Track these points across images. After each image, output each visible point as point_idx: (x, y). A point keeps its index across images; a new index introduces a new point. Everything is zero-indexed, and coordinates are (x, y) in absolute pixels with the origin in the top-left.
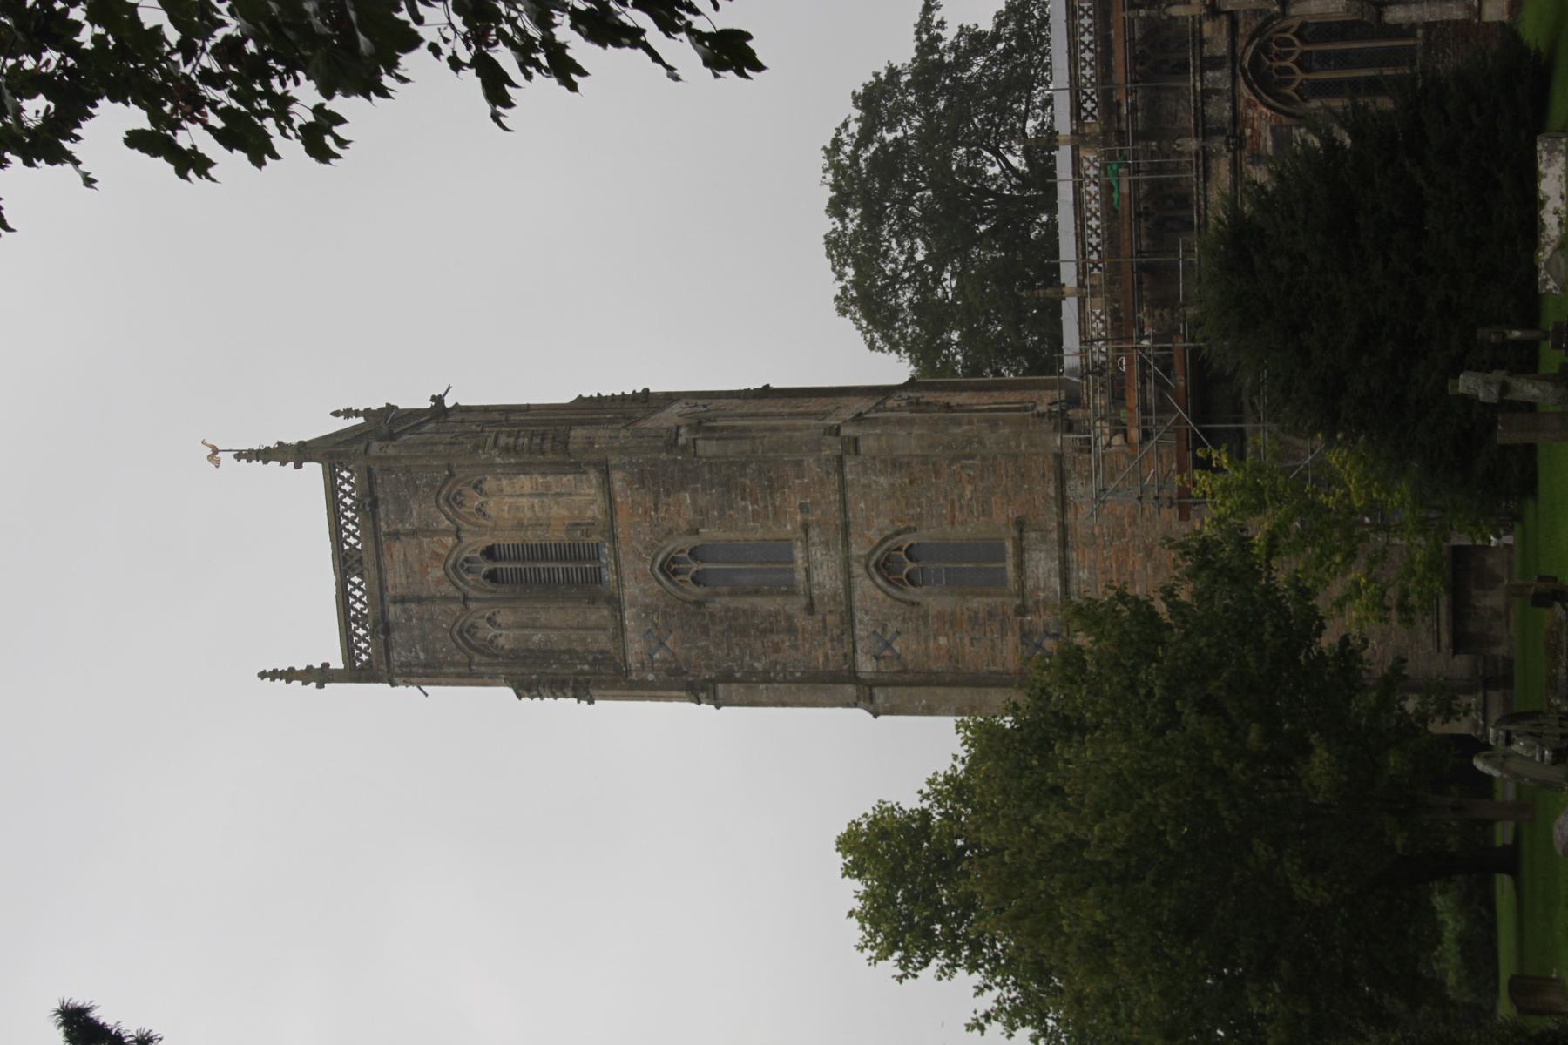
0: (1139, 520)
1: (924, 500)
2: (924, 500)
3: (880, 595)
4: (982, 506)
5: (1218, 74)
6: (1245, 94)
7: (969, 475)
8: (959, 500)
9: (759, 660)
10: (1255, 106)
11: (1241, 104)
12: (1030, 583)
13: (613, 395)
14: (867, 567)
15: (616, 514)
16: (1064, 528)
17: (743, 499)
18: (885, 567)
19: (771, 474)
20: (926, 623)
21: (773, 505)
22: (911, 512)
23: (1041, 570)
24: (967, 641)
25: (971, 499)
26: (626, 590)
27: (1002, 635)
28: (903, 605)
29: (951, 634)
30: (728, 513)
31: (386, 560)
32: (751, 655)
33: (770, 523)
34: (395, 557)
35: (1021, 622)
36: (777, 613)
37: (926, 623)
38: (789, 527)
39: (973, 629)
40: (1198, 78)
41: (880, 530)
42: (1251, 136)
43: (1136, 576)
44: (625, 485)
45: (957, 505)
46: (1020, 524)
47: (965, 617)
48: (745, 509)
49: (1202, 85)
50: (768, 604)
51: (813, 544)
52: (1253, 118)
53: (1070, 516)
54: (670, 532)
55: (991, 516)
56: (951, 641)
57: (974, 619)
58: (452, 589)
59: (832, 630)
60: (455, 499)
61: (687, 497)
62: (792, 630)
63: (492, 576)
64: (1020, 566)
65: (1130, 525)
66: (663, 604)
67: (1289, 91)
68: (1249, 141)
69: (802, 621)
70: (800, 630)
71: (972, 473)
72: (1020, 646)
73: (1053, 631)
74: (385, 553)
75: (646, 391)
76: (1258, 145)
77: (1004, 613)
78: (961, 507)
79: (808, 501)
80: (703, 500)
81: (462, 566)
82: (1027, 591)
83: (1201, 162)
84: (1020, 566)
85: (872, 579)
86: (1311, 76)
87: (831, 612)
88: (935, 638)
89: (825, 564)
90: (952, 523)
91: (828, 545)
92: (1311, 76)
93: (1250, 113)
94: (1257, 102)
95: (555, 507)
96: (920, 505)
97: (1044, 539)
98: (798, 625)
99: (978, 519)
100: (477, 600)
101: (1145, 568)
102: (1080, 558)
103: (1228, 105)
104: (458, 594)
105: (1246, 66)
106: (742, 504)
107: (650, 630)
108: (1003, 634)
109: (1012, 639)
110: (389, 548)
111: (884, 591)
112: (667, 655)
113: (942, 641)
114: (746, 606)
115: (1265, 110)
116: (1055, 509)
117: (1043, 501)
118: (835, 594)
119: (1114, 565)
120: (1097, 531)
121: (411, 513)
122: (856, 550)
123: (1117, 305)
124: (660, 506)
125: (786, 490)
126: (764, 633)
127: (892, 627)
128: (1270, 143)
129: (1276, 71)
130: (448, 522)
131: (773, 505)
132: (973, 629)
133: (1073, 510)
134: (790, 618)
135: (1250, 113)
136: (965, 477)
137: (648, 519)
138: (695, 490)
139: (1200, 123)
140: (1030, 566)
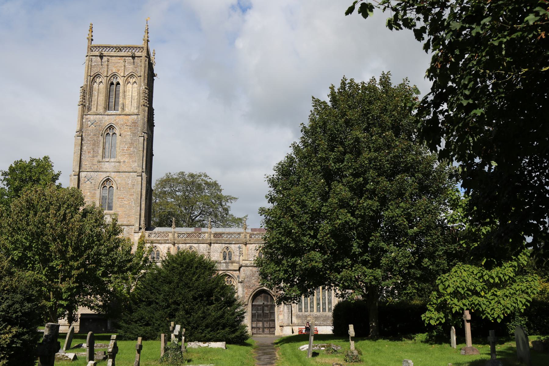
20: (93, 190)
37: (93, 190)
48: (125, 147)
61: (129, 133)
62: (93, 157)
63: (112, 84)
69: (96, 160)
75: (154, 126)
80: (128, 137)
106: (126, 147)
112: (89, 125)
113: (89, 194)
127: (93, 181)
134: (97, 156)
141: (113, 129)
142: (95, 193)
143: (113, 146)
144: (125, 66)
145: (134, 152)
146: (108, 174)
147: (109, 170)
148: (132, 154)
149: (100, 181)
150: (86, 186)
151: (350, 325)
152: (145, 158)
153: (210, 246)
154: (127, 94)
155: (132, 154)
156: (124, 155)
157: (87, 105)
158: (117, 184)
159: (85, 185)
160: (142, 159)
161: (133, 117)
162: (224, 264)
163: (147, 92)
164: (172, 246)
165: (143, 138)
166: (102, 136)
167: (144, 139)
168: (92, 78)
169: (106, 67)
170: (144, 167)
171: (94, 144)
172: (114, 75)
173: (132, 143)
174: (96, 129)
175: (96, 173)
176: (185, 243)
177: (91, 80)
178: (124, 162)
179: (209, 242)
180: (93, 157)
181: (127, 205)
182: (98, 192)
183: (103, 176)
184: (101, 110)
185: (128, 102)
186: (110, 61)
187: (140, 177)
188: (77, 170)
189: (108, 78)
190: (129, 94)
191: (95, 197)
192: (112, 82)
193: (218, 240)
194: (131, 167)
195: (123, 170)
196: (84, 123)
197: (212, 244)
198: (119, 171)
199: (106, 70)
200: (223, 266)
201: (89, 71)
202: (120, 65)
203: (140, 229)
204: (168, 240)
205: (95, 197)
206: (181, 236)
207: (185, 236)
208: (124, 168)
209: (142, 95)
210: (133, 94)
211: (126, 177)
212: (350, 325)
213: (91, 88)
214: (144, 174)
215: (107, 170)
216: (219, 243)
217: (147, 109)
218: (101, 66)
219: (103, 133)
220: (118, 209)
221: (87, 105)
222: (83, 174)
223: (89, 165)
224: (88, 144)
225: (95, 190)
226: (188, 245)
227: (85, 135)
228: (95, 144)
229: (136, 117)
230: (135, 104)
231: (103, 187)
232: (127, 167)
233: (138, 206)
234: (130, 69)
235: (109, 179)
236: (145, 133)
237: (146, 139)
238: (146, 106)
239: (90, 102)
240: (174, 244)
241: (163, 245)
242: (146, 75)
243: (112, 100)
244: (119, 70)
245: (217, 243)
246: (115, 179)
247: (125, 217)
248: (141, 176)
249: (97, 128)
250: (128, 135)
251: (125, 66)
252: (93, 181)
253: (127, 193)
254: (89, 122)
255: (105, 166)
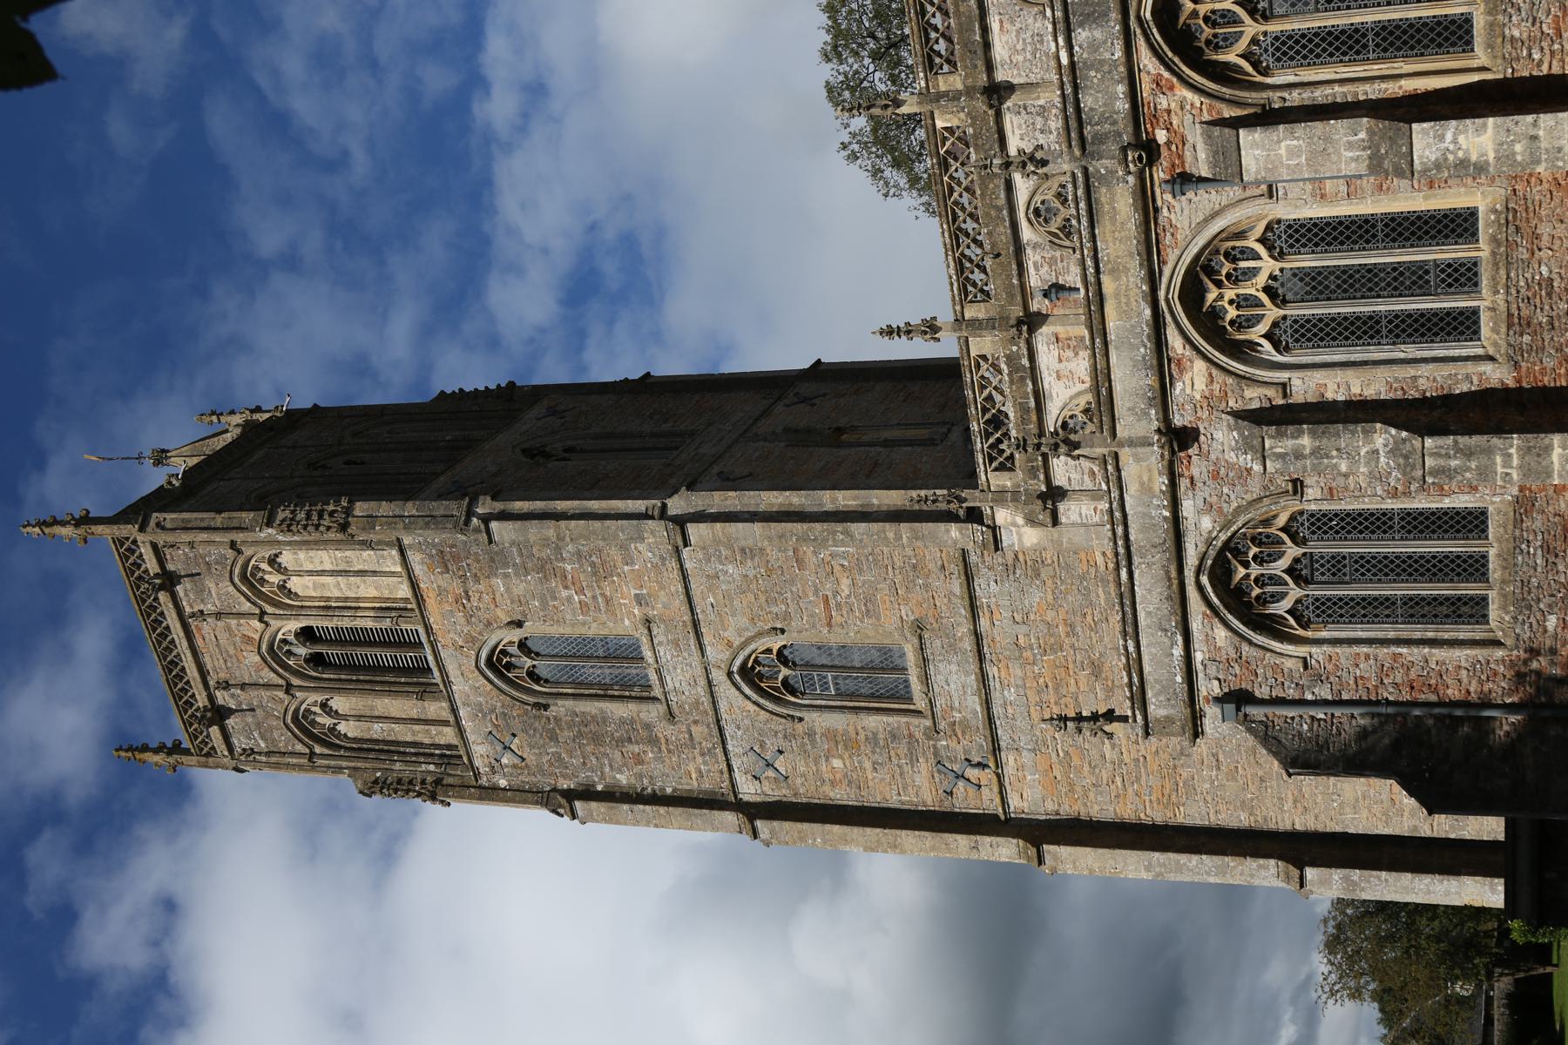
0: (1079, 629)
1: (789, 595)
2: (789, 595)
3: (752, 707)
4: (865, 605)
5: (1098, 34)
6: (1150, 67)
7: (842, 566)
8: (834, 596)
9: (621, 772)
10: (1171, 88)
11: (1146, 87)
12: (940, 703)
13: (476, 389)
14: (730, 674)
15: (424, 601)
16: (978, 637)
17: (566, 587)
18: (750, 674)
19: (594, 558)
20: (813, 742)
21: (603, 595)
22: (775, 609)
23: (953, 686)
24: (868, 765)
25: (849, 596)
26: (454, 688)
27: (911, 760)
28: (783, 720)
29: (846, 756)
30: (550, 603)
31: (199, 642)
32: (611, 766)
33: (604, 617)
34: (207, 640)
35: (935, 747)
36: (632, 721)
37: (813, 742)
38: (627, 622)
39: (873, 752)
40: (1061, 41)
41: (739, 633)
42: (1168, 143)
43: (1081, 698)
44: (425, 568)
45: (832, 602)
46: (919, 628)
47: (862, 737)
48: (569, 599)
49: (1071, 55)
50: (619, 710)
51: (660, 643)
52: (1169, 112)
53: (984, 623)
54: (489, 624)
55: (878, 619)
56: (848, 764)
57: (873, 739)
58: (272, 675)
59: (700, 743)
60: (253, 575)
61: (498, 583)
62: (653, 741)
63: (317, 660)
64: (926, 679)
65: (1068, 635)
66: (499, 704)
67: (1231, 57)
68: (1164, 152)
69: (664, 730)
70: (663, 741)
71: (846, 563)
72: (936, 775)
73: (976, 759)
74: (197, 635)
75: (511, 384)
76: (1181, 157)
77: (911, 736)
78: (838, 605)
79: (645, 591)
80: (519, 588)
81: (280, 648)
82: (938, 709)
83: (1080, 192)
84: (926, 679)
85: (738, 689)
86: (1274, 27)
87: (696, 722)
88: (827, 760)
89: (679, 666)
90: (829, 625)
91: (678, 645)
92: (1274, 27)
93: (1163, 102)
94: (1175, 80)
95: (362, 586)
96: (785, 601)
97: (953, 647)
98: (660, 735)
99: (862, 622)
100: (300, 688)
101: (1093, 690)
102: (1003, 675)
103: (1121, 89)
104: (281, 682)
105: (1148, 15)
106: (565, 593)
107: (490, 732)
108: (913, 760)
109: (924, 767)
110: (199, 629)
111: (755, 703)
112: (517, 761)
113: (837, 763)
114: (594, 711)
115: (1189, 95)
116: (963, 612)
117: (946, 600)
118: (697, 702)
119: (1050, 684)
120: (1021, 641)
121: (210, 592)
122: (715, 653)
123: (1015, 348)
124: (470, 593)
125: (615, 578)
126: (620, 743)
127: (771, 745)
128: (1202, 155)
129: (1206, 19)
130: (249, 604)
131: (603, 595)
132: (873, 752)
133: (987, 614)
134: (648, 727)
135: (1163, 102)
136: (837, 568)
137: (461, 608)
138: (506, 576)
139: (1073, 124)
140: (938, 680)
141: (503, 652)
142: (830, 735)
143: (580, 650)
144: (218, 615)
145: (579, 554)
146: (719, 676)
147: (699, 671)
148: (593, 565)
149: (763, 715)
150: (803, 775)
151: (1499, 885)
152: (595, 505)
153: (1010, 88)
154: (337, 594)
155: (593, 565)
156: (608, 601)
157: (432, 768)
158: (760, 634)
159: (799, 781)
160: (597, 524)
161: (418, 570)
162: (1081, 35)
163: (287, 513)
164: (1044, 333)
165: (494, 525)
166: (546, 707)
167: (504, 516)
168: (318, 749)
169: (253, 693)
170: (639, 505)
171: (597, 739)
172: (275, 654)
173: (541, 569)
174: (524, 731)
175: (729, 731)
176: (1019, 249)
177: (326, 751)
178: (639, 600)
179: (980, 104)
180: (653, 741)
181: (860, 579)
182: (820, 721)
183: (735, 702)
184: (436, 708)
185: (367, 589)
186: (223, 676)
187: (692, 529)
188: (730, 817)
189: (296, 681)
190: (335, 588)
191: (846, 733)
192: (307, 661)
193: (966, 44)
194: (655, 566)
195: (679, 602)
196: (516, 782)
197: (1001, 76)
198: (689, 624)
199: (265, 694)
200: (1093, 46)
201: (295, 761)
202: (224, 639)
203: (974, 516)
204: (1011, 359)
205: (846, 733)
206: (977, 276)
207: (974, 252)
208: (668, 602)
209: (315, 536)
210: (328, 567)
211: (711, 589)
212: (1499, 885)
213: (364, 749)
214: (676, 505)
215: (702, 682)
216: (985, 30)
217: (360, 508)
218: (259, 712)
219: (531, 700)
220: (890, 621)
221: (432, 768)
222: (749, 790)
223: (699, 760)
224: (602, 765)
225: (811, 734)
226: (1027, 233)
227: (564, 776)
228: (593, 734)
229: (415, 558)
230: (364, 559)
231: (793, 692)
232: (662, 587)
233: (846, 533)
234: (220, 592)
235: (743, 670)
236: (470, 514)
237: (499, 506)
238: (348, 512)
239: (421, 751)
240: (1032, 322)
241: (1048, 381)
242: (219, 520)
243: (386, 655)
244: (247, 639)
245: (987, 45)
246: (736, 643)
247: (926, 586)
248: (681, 522)
249: (516, 725)
250: (508, 590)
251: (218, 615)
252: (771, 745)
253: (792, 582)
254: (505, 761)
255: (686, 688)
